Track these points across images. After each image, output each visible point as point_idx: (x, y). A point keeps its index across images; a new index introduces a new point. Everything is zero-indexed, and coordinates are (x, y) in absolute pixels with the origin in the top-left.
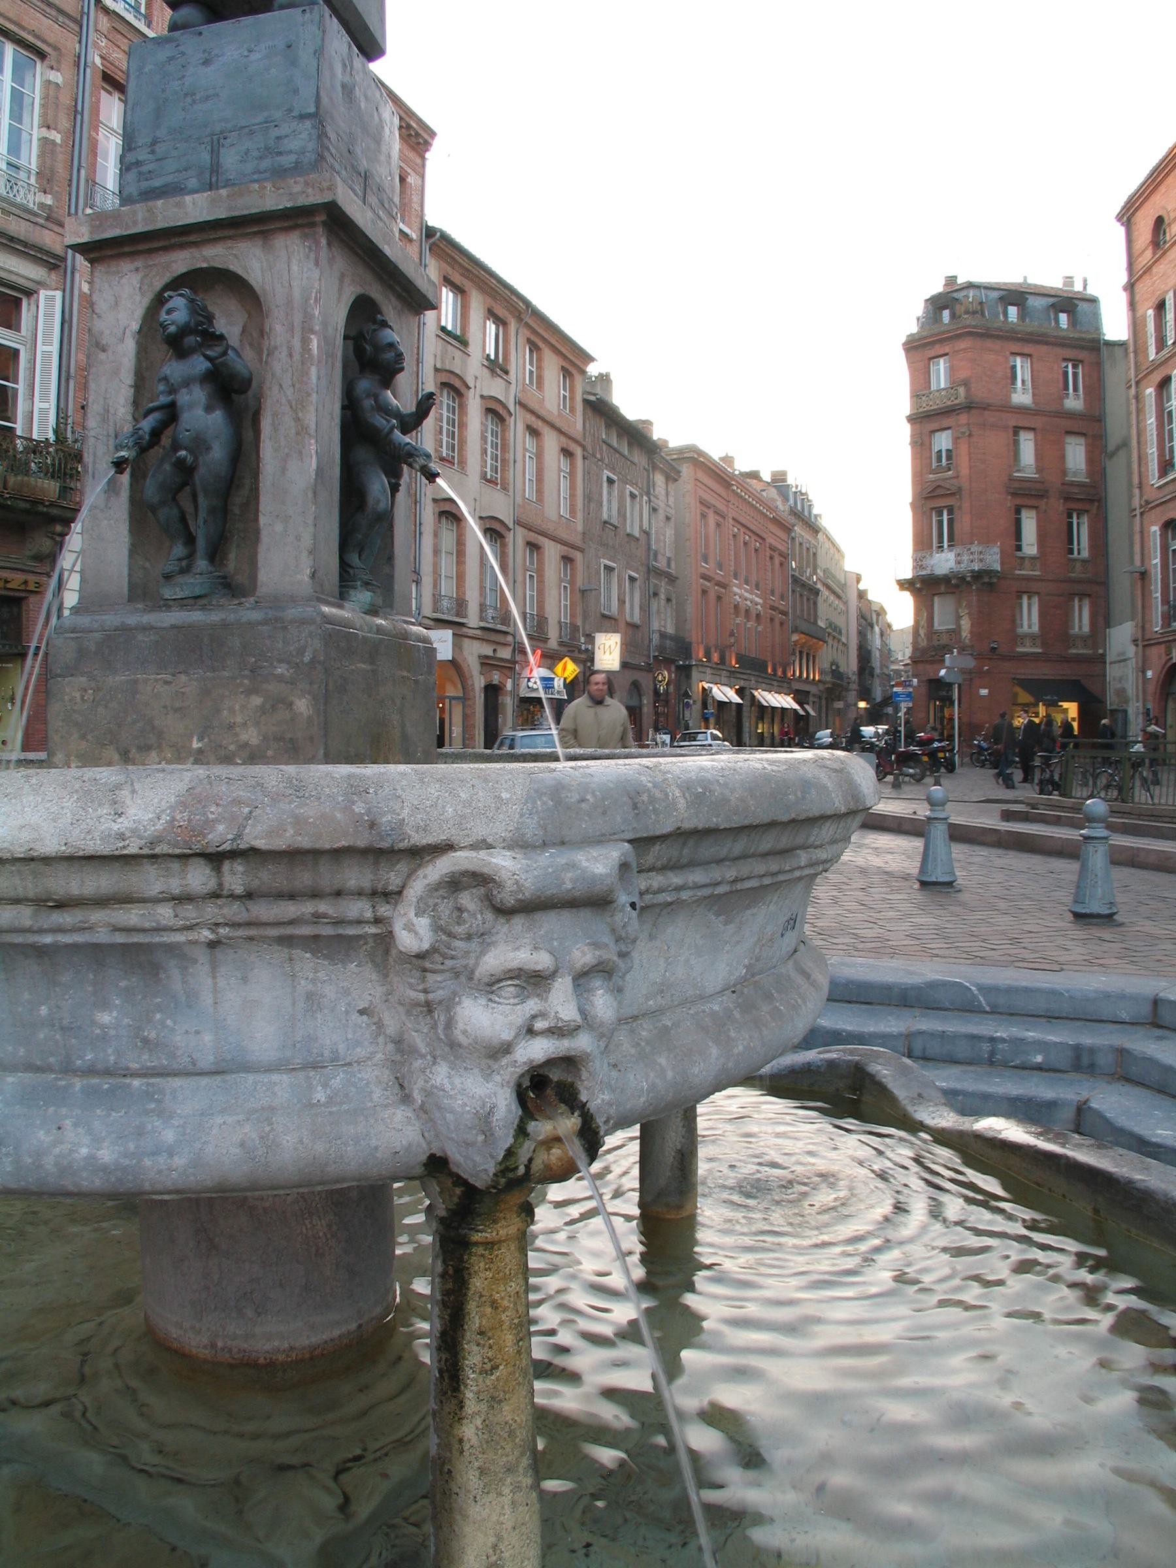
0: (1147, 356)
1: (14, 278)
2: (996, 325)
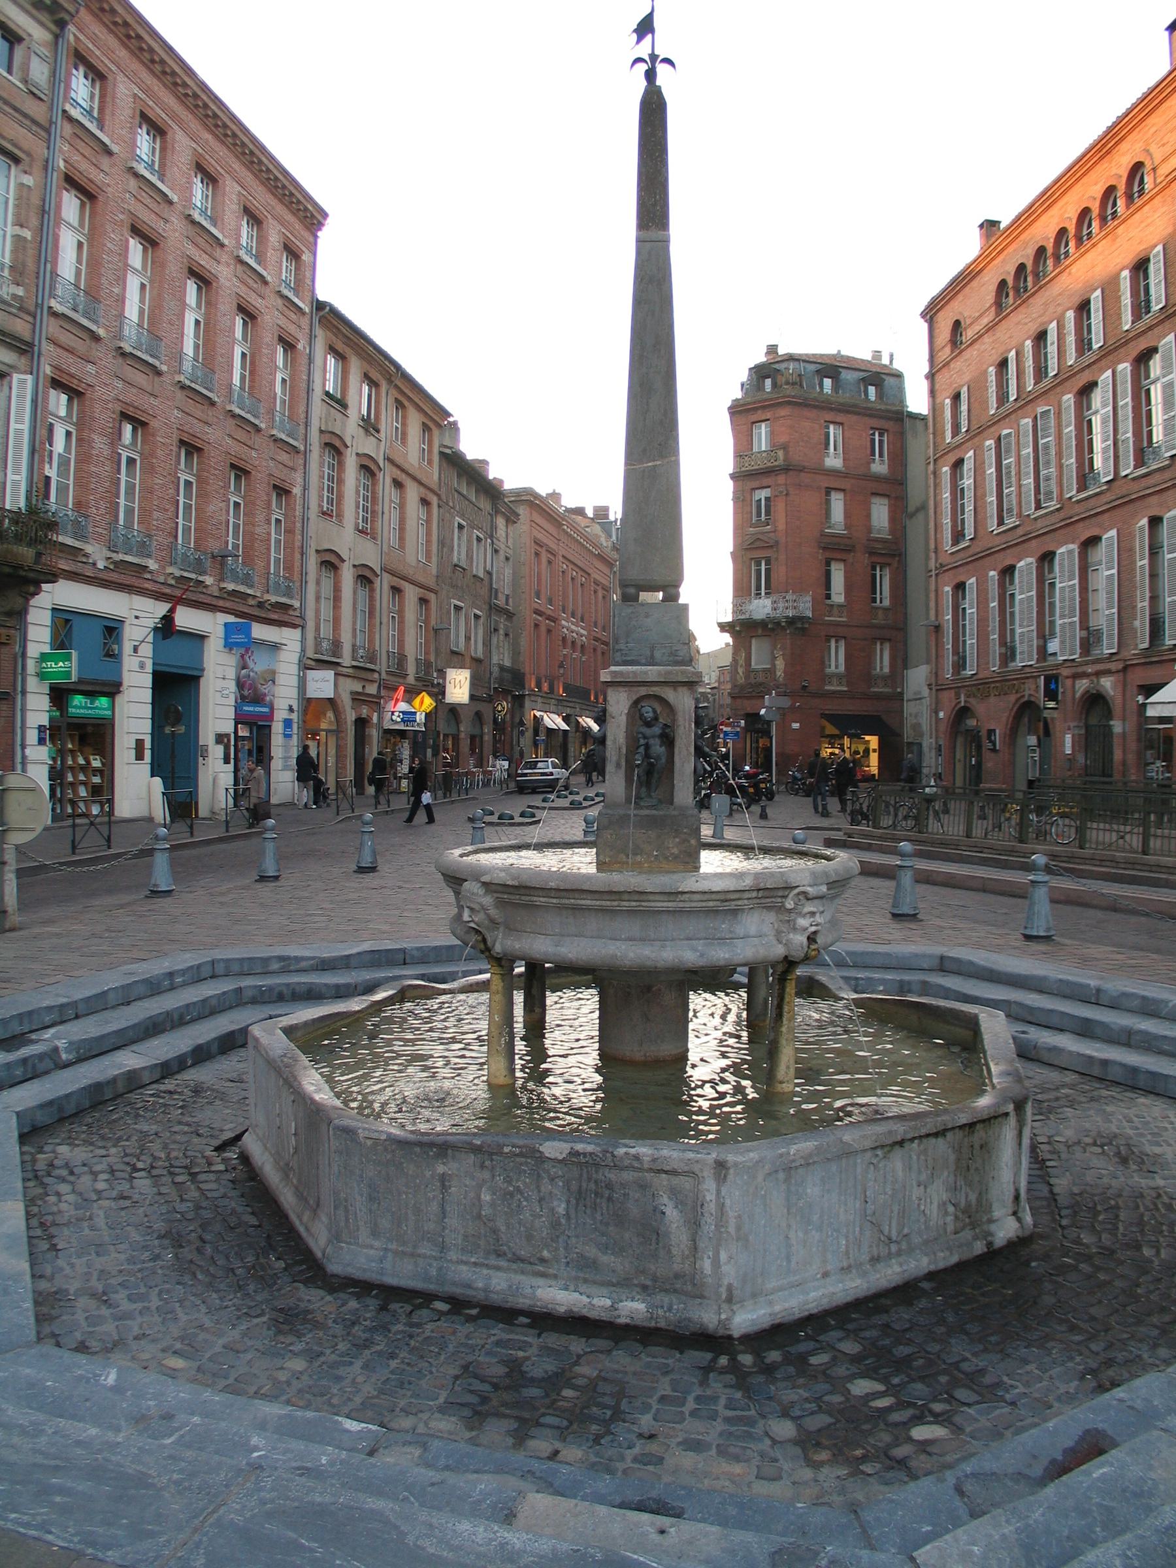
0: (944, 438)
2: (812, 396)
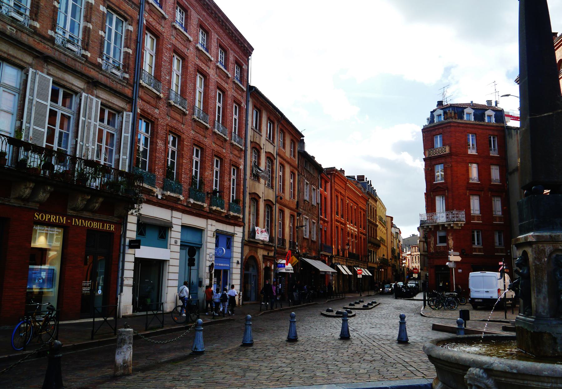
1: (114, 106)
